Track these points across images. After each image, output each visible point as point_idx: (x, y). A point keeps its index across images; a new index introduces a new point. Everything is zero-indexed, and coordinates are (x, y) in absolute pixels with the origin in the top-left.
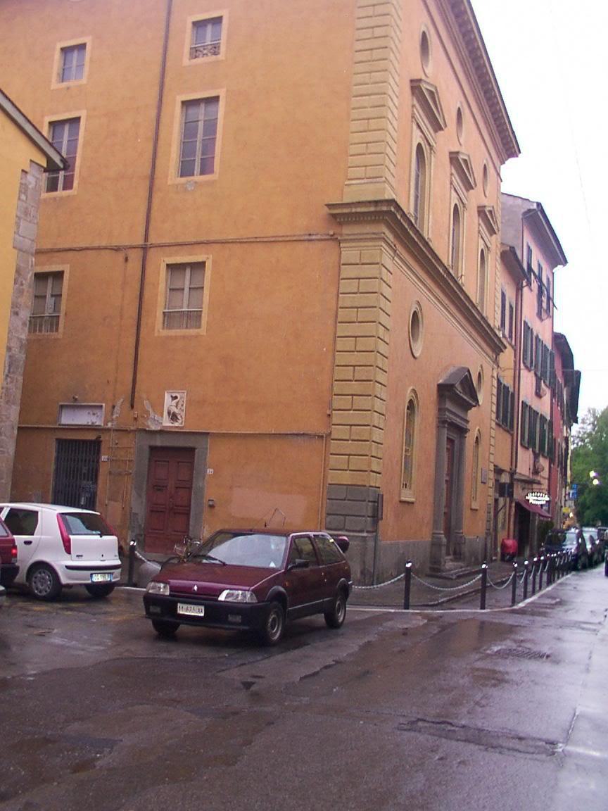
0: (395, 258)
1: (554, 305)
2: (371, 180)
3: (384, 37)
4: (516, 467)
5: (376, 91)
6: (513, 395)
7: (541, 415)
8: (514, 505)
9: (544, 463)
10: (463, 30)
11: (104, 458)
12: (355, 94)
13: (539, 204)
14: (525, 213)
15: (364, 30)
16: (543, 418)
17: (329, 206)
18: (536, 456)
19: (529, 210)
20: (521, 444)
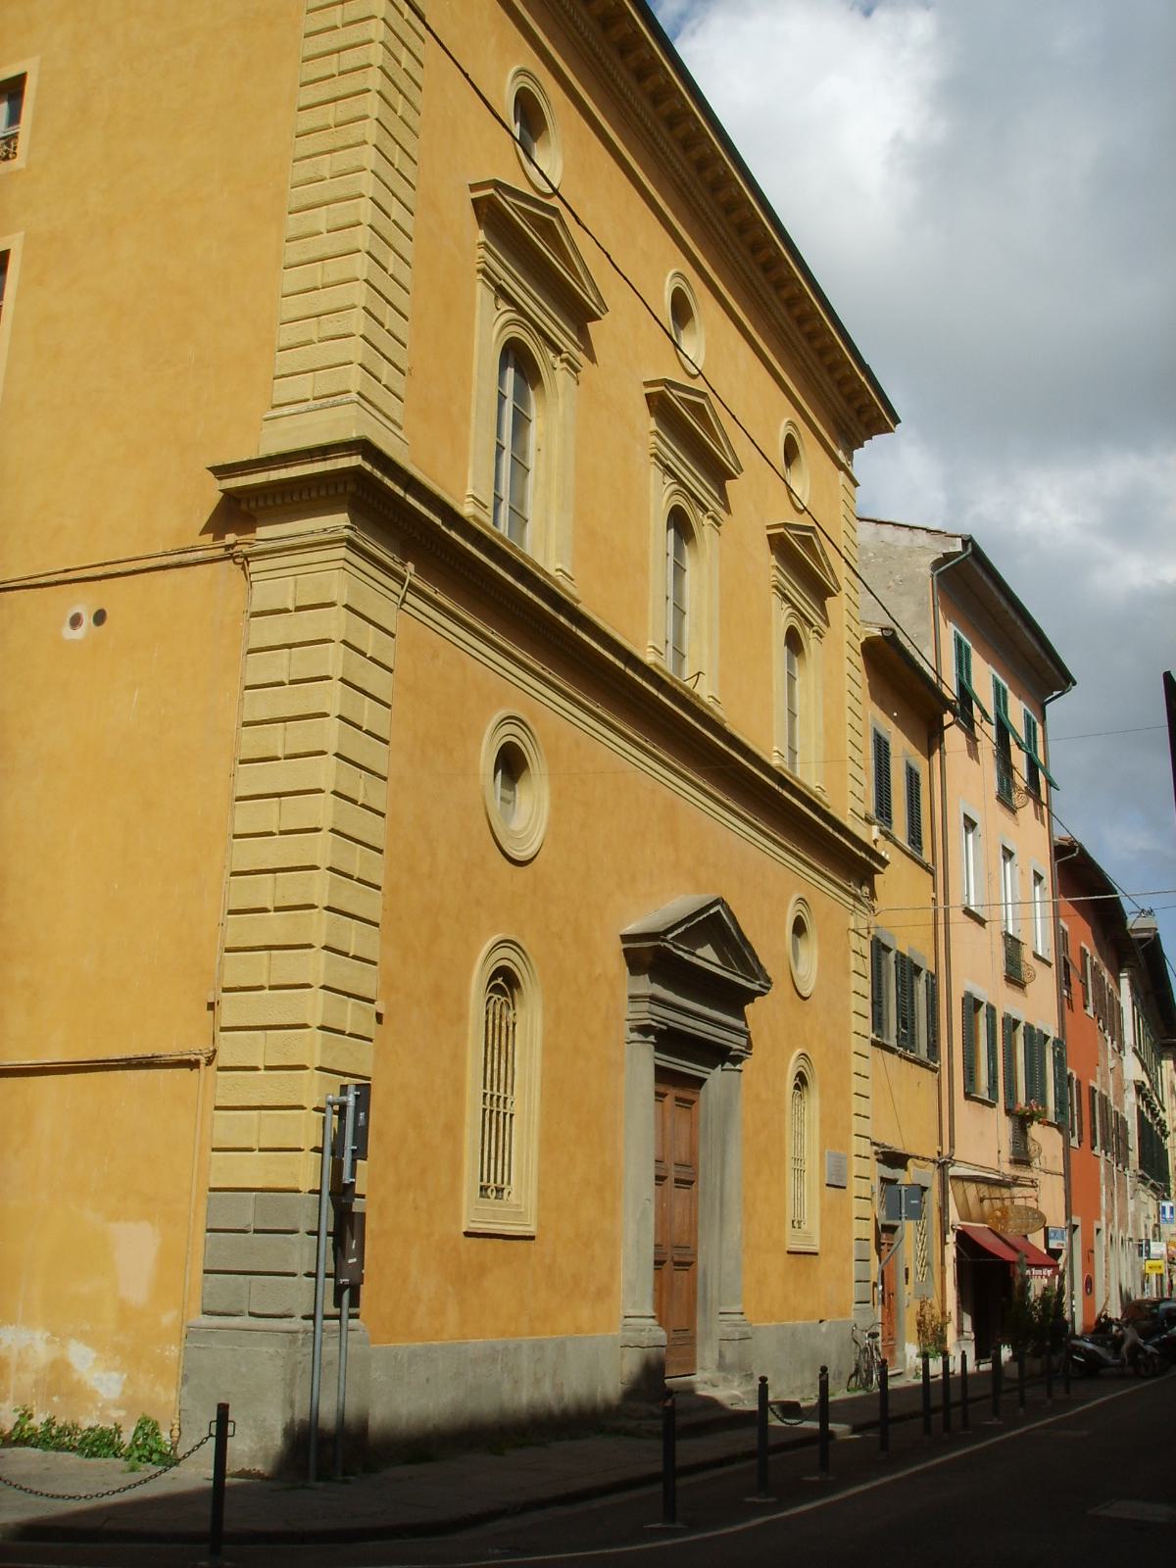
0: (410, 598)
1: (1050, 783)
2: (324, 400)
3: (363, 67)
4: (952, 1146)
5: (343, 193)
6: (933, 977)
7: (1029, 1028)
8: (951, 1238)
9: (1046, 1141)
10: (856, 405)
11: (883, 854)
12: (294, 206)
13: (968, 541)
14: (936, 564)
15: (352, 98)
16: (1035, 1040)
17: (222, 471)
18: (1022, 1122)
19: (947, 557)
20: (968, 1096)
